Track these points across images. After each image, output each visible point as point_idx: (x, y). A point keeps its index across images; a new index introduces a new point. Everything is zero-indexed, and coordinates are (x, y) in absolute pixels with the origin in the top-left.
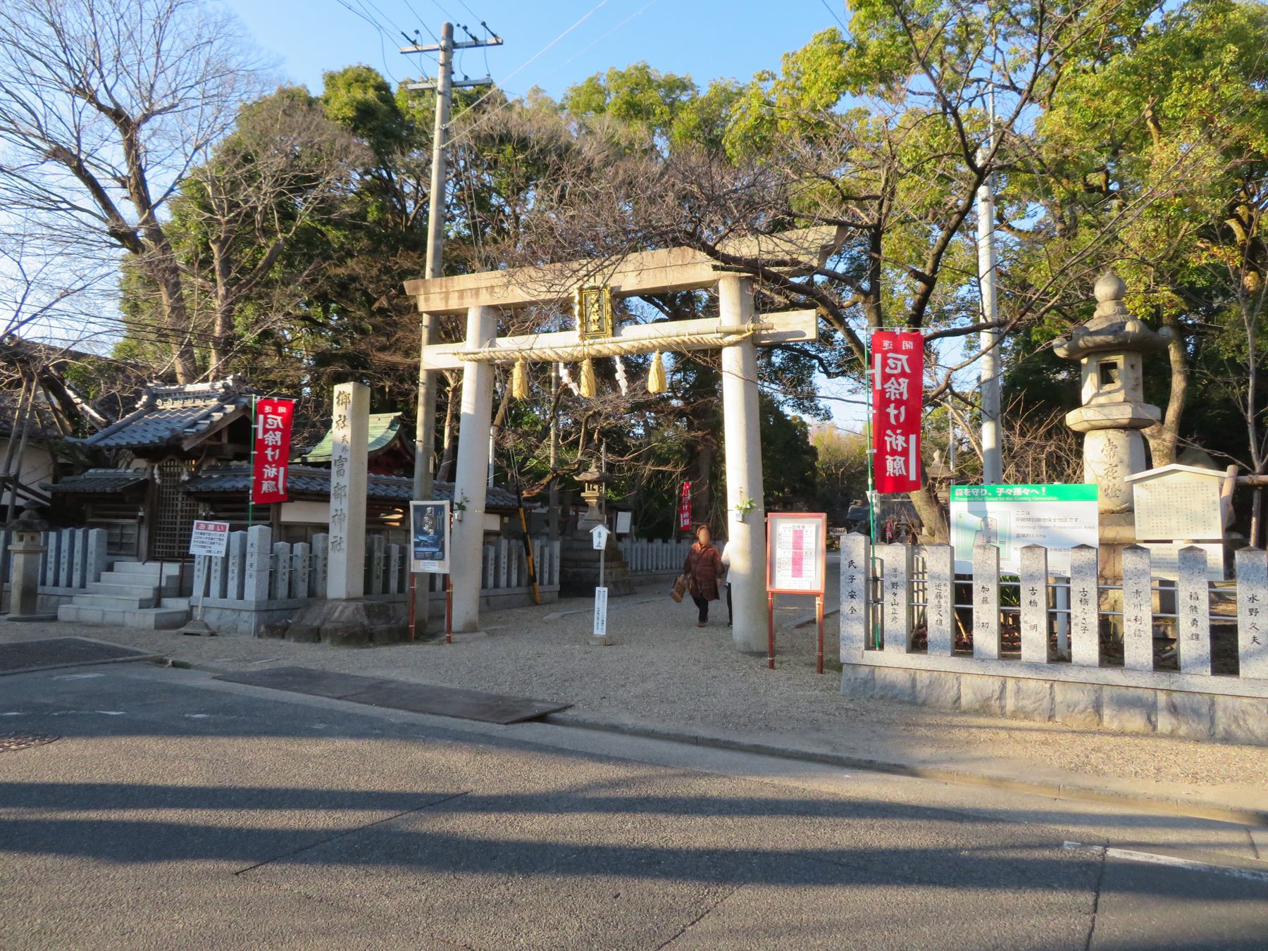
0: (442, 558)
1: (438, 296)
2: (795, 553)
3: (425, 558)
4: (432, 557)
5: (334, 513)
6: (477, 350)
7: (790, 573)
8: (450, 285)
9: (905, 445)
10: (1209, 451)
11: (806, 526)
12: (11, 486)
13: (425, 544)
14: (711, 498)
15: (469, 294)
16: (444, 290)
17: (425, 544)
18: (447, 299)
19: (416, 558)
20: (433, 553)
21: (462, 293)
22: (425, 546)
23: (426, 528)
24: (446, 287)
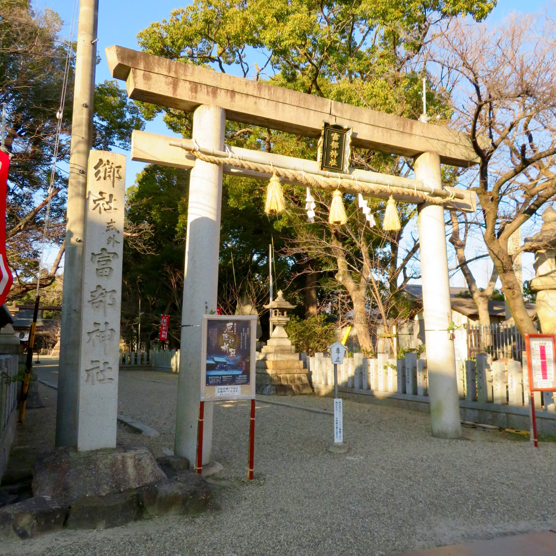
0: (248, 381)
1: (163, 79)
2: (542, 362)
3: (222, 383)
4: (232, 381)
5: (92, 328)
6: (217, 152)
7: (541, 376)
8: (181, 71)
9: (392, 255)
10: (348, 264)
11: (547, 342)
12: (173, 281)
13: (223, 366)
14: (59, 441)
15: (204, 89)
16: (172, 74)
17: (223, 366)
18: (175, 84)
19: (208, 383)
20: (234, 377)
21: (195, 86)
22: (222, 368)
23: (224, 347)
24: (176, 72)
